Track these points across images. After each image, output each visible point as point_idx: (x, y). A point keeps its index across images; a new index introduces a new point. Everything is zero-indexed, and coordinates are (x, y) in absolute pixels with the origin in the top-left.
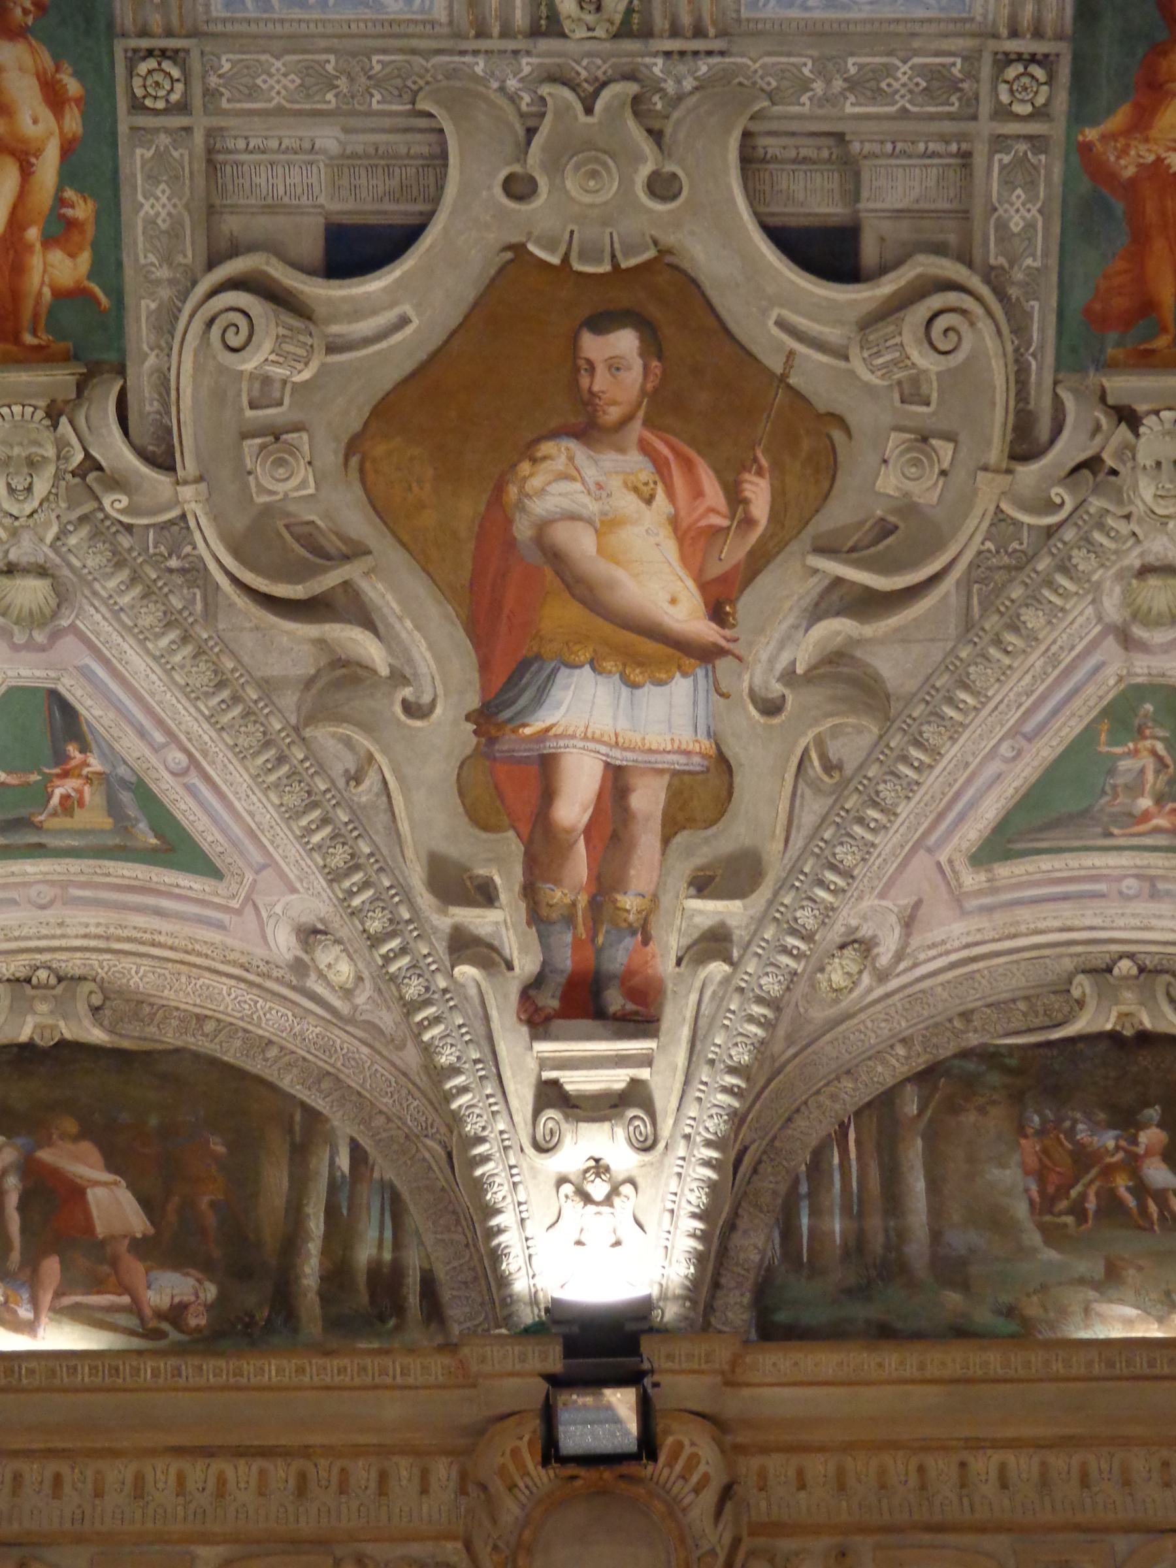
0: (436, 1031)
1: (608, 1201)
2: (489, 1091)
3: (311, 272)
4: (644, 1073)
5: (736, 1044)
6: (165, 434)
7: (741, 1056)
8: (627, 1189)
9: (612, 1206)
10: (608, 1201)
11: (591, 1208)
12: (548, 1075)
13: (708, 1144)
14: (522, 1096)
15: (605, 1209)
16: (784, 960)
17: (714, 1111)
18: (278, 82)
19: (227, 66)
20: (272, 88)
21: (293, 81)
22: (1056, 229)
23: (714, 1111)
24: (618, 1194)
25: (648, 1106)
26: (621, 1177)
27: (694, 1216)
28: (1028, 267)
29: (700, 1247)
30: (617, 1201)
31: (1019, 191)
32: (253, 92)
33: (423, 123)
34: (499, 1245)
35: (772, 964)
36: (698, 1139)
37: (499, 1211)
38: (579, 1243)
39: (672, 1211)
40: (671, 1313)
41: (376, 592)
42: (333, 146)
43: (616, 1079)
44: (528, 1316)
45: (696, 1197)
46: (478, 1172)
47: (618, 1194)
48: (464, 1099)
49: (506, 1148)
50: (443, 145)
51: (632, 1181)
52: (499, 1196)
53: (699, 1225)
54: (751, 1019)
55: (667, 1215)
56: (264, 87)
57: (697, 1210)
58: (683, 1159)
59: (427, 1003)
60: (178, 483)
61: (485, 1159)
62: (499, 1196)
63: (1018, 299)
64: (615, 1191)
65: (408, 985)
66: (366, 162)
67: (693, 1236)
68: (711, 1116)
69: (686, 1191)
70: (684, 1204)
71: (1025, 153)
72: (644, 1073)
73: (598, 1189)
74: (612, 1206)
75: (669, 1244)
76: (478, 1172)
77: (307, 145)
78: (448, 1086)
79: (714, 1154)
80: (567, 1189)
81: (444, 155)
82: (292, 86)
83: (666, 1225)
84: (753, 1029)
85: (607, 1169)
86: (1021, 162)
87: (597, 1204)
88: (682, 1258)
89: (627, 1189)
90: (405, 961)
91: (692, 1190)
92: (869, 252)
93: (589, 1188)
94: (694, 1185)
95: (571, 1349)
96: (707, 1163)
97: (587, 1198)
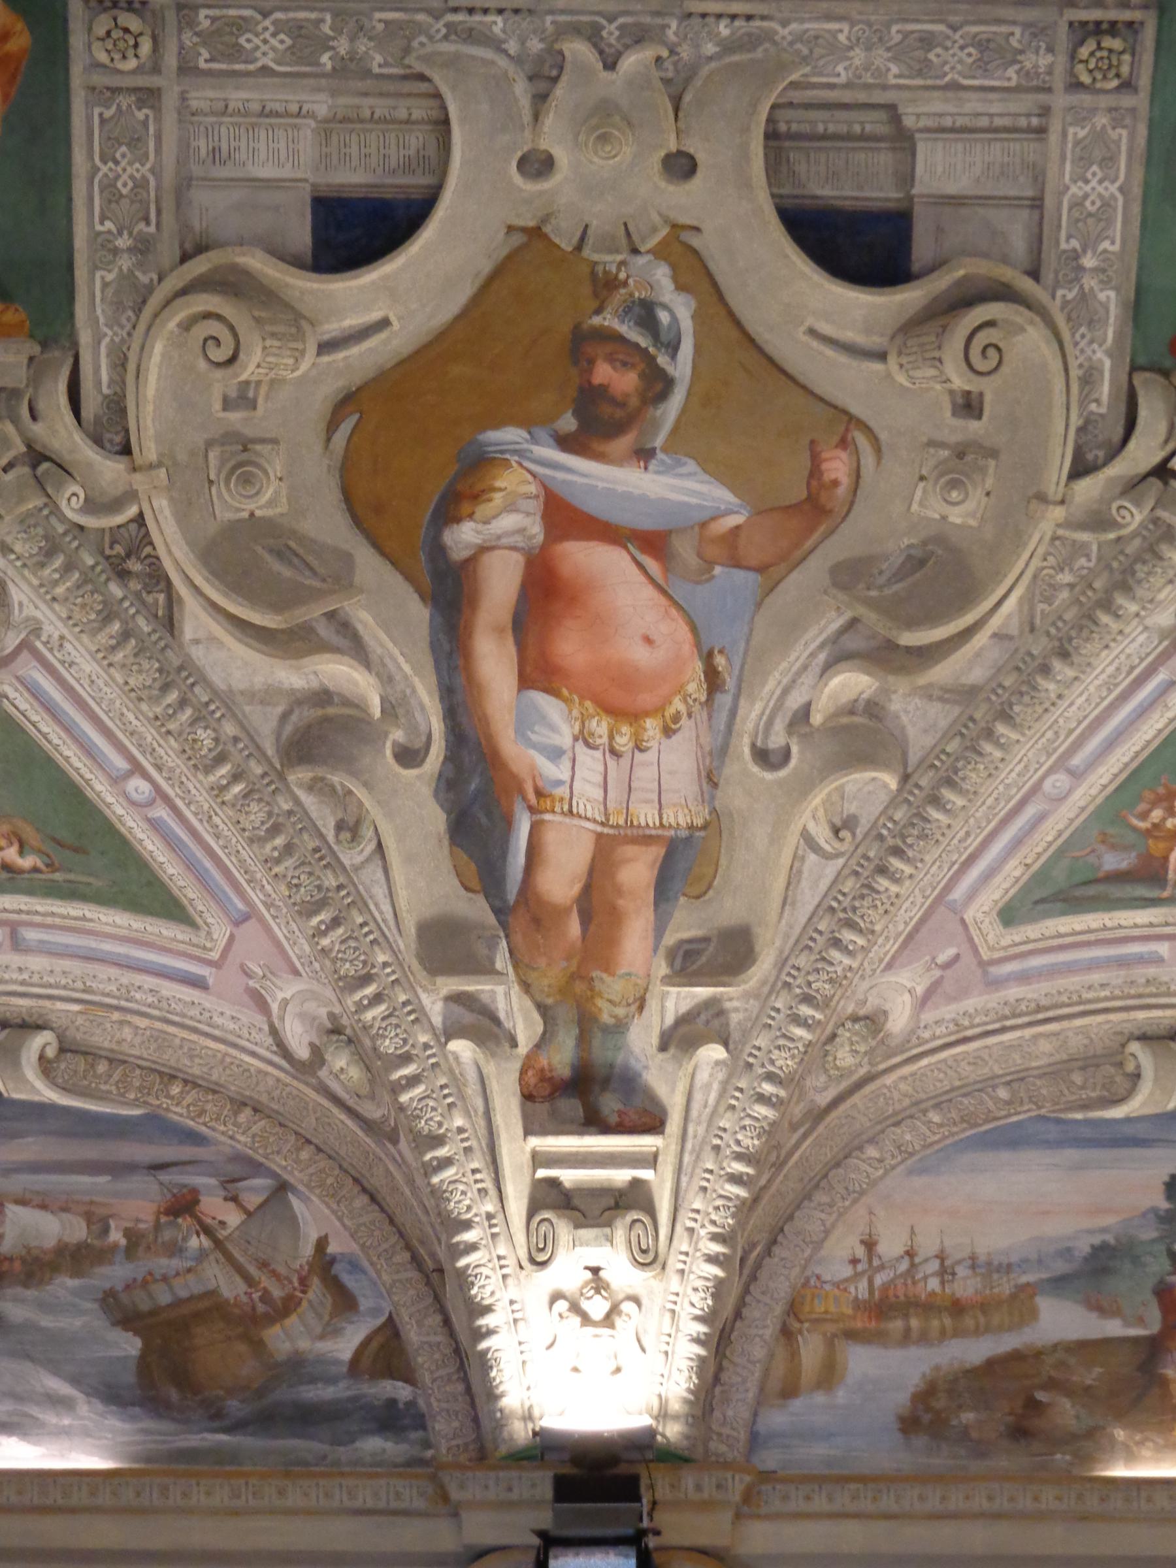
0: (419, 1090)
1: (608, 1320)
2: (475, 1165)
3: (296, 262)
4: (646, 1174)
5: (744, 1128)
6: (117, 407)
7: (750, 1142)
8: (628, 1307)
9: (612, 1326)
10: (608, 1320)
11: (590, 1330)
12: (542, 1173)
13: (715, 1237)
14: (517, 1206)
15: (606, 1331)
16: (799, 1032)
17: (719, 1202)
18: (265, 41)
19: (205, 24)
20: (257, 48)
21: (282, 42)
22: (1136, 209)
23: (719, 1202)
24: (620, 1313)
25: (651, 1210)
26: (621, 1296)
27: (697, 1318)
28: (1105, 251)
29: (702, 1351)
30: (619, 1322)
31: (1095, 168)
32: (235, 52)
33: (423, 87)
34: (488, 1349)
35: (784, 1036)
36: (703, 1232)
37: (488, 1309)
38: (576, 1370)
39: (673, 1312)
40: (673, 1431)
41: (364, 619)
42: (322, 110)
43: (621, 1176)
44: (520, 1433)
45: (703, 1302)
46: (462, 1263)
47: (620, 1313)
48: (449, 1173)
49: (494, 1236)
50: (444, 108)
51: (636, 1300)
52: (463, 1206)
53: (702, 1329)
54: (762, 1099)
55: (668, 1315)
56: (248, 46)
57: (699, 1313)
58: (687, 1254)
59: (406, 1059)
60: (134, 470)
61: (472, 1247)
62: (463, 1206)
63: (1092, 289)
64: (614, 1310)
65: (384, 1037)
66: (359, 126)
67: (697, 1340)
68: (717, 1208)
69: (690, 1291)
70: (686, 1305)
71: (1104, 126)
72: (646, 1174)
73: (597, 1307)
74: (612, 1326)
75: (669, 1349)
76: (462, 1263)
77: (294, 108)
78: (428, 1157)
79: (716, 1248)
80: (561, 1305)
81: (446, 122)
82: (280, 47)
83: (667, 1328)
84: (762, 1110)
85: (607, 1287)
86: (1099, 136)
87: (595, 1324)
88: (685, 1364)
89: (628, 1307)
90: (381, 1009)
91: (696, 1290)
92: (922, 249)
93: (585, 1305)
94: (700, 1284)
95: (565, 1490)
96: (711, 1259)
97: (586, 1319)
